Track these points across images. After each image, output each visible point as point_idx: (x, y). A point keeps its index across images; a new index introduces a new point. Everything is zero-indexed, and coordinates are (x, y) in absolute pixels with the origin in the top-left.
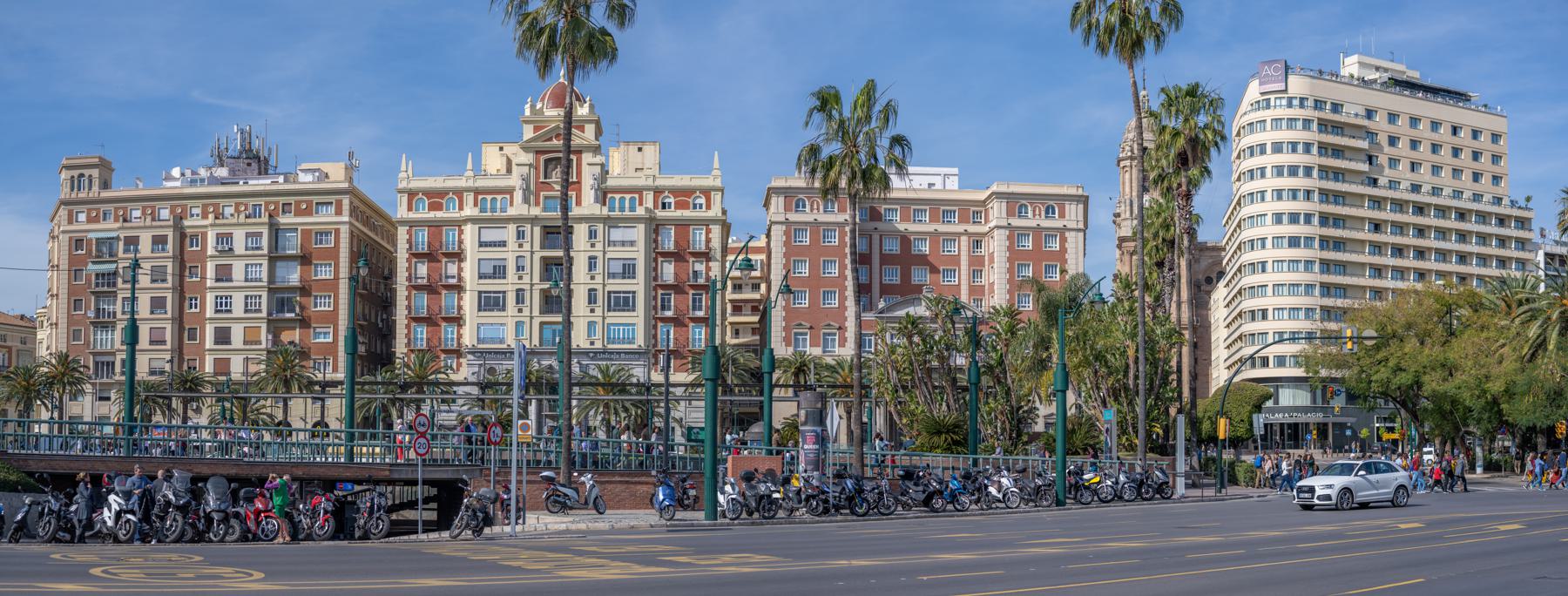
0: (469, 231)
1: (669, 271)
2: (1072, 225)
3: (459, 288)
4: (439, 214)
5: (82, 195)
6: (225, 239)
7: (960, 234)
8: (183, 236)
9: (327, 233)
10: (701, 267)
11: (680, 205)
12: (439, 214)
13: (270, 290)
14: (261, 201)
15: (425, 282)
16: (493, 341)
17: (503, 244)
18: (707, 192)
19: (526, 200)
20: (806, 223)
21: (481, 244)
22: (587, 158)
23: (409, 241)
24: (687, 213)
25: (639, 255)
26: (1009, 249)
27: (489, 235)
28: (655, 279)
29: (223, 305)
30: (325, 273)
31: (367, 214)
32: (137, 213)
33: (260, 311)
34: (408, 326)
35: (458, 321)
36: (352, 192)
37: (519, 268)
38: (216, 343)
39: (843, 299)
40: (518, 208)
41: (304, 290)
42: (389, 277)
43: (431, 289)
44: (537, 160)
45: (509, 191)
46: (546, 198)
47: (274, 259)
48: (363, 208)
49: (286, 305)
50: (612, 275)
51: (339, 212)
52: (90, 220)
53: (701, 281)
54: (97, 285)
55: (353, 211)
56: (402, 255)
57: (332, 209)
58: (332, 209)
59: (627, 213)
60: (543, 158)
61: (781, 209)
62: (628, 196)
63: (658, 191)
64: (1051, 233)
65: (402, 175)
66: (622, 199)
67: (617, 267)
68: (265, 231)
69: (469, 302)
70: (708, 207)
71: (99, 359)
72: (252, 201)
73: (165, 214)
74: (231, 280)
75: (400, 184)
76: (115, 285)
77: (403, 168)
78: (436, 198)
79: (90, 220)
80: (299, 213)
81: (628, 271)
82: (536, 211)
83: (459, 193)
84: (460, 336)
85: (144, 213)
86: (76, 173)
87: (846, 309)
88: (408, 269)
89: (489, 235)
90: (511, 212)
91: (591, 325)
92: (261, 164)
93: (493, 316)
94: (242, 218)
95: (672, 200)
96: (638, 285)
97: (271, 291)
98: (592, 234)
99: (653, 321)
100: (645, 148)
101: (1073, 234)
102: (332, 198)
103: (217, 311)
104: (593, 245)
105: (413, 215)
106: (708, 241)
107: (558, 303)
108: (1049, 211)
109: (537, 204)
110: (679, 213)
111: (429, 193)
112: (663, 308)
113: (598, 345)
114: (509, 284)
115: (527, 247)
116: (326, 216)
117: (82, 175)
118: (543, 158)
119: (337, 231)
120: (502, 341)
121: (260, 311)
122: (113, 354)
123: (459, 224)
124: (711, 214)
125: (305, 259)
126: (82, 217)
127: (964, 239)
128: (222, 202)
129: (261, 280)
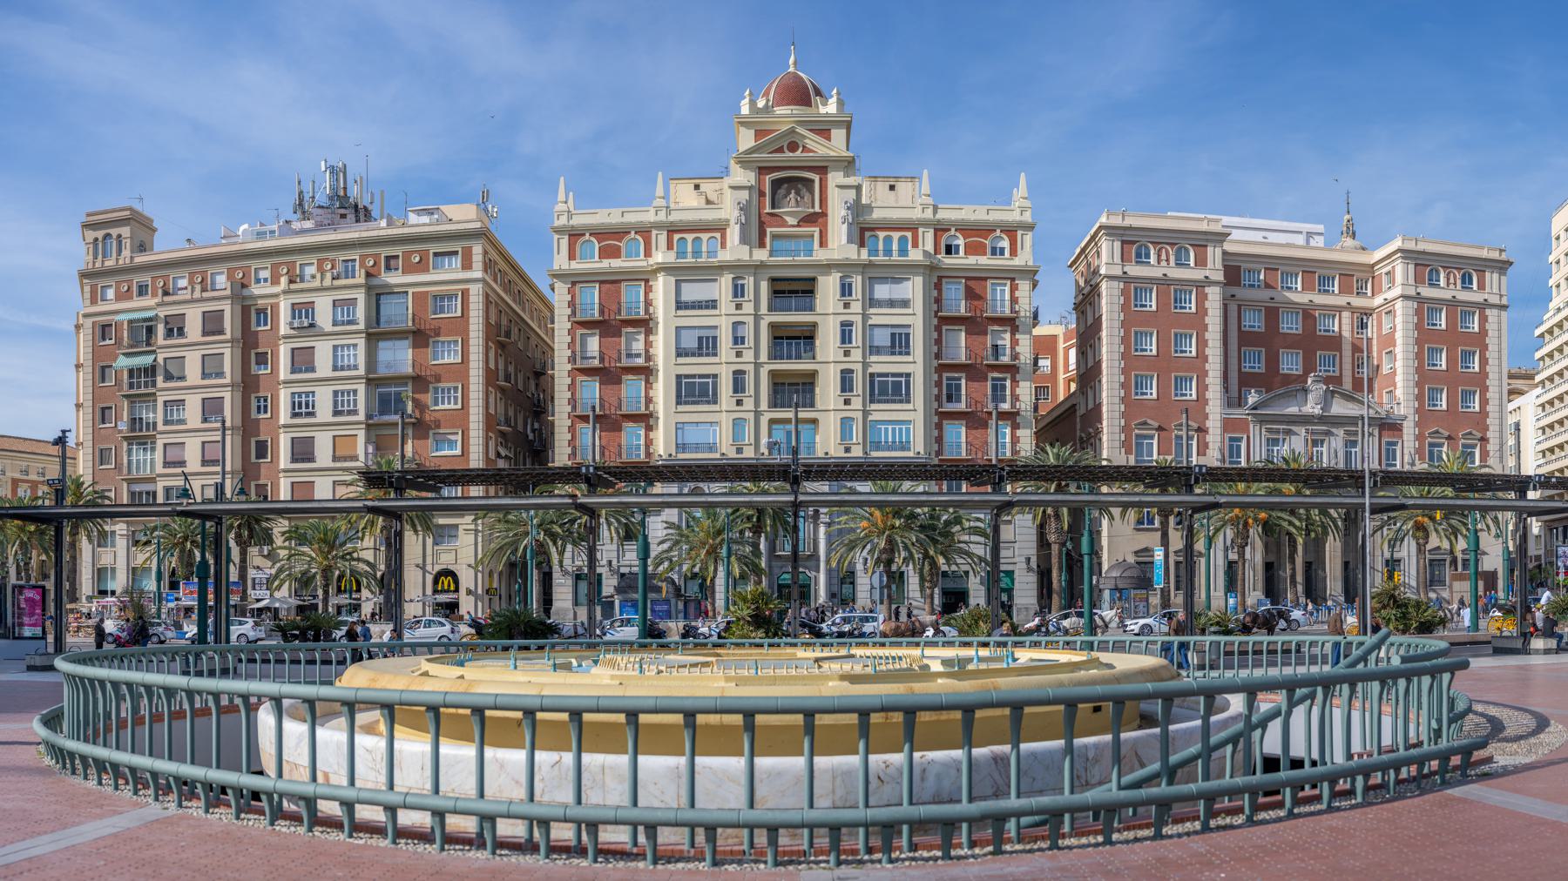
0: (662, 288)
1: (960, 345)
2: (1494, 300)
3: (647, 372)
4: (616, 263)
5: (110, 263)
6: (303, 311)
7: (1340, 309)
8: (246, 311)
9: (451, 297)
10: (1006, 340)
11: (972, 249)
12: (616, 263)
13: (369, 381)
14: (355, 255)
15: (596, 363)
16: (697, 448)
17: (712, 304)
18: (1011, 231)
19: (744, 240)
20: (1151, 280)
21: (680, 305)
22: (835, 178)
23: (572, 304)
24: (984, 261)
25: (915, 321)
26: (1418, 327)
27: (691, 292)
28: (938, 356)
29: (303, 408)
30: (449, 357)
31: (507, 276)
32: (183, 283)
33: (355, 412)
34: (572, 429)
35: (646, 419)
36: (481, 234)
37: (738, 340)
38: (294, 460)
39: (1202, 388)
40: (734, 250)
41: (420, 381)
42: (540, 374)
43: (607, 326)
44: (760, 181)
45: (720, 228)
46: (775, 237)
47: (374, 337)
48: (502, 265)
49: (394, 404)
50: (875, 350)
51: (467, 265)
52: (119, 297)
53: (1005, 359)
54: (131, 386)
55: (488, 265)
56: (562, 325)
57: (457, 262)
58: (457, 262)
59: (895, 257)
60: (768, 178)
61: (1117, 259)
62: (896, 235)
63: (940, 229)
64: (1469, 308)
65: (561, 207)
66: (888, 240)
67: (882, 338)
68: (361, 296)
69: (662, 392)
70: (1014, 253)
71: (137, 488)
72: (342, 256)
73: (222, 280)
74: (313, 370)
75: (550, 229)
76: (154, 384)
77: (561, 197)
78: (611, 239)
79: (119, 297)
80: (407, 270)
81: (899, 343)
82: (761, 255)
83: (645, 231)
84: (649, 443)
85: (191, 282)
86: (100, 234)
87: (1206, 402)
88: (571, 345)
89: (691, 292)
90: (725, 256)
91: (846, 423)
92: (362, 214)
93: (696, 412)
94: (328, 282)
95: (961, 242)
96: (914, 364)
97: (370, 382)
98: (846, 290)
99: (940, 418)
100: (900, 186)
101: (1495, 312)
102: (457, 246)
103: (295, 415)
104: (847, 305)
105: (575, 266)
106: (1014, 300)
107: (794, 390)
108: (1466, 281)
109: (762, 245)
110: (972, 260)
111: (601, 233)
112: (950, 399)
113: (857, 452)
114: (722, 365)
115: (748, 308)
116: (449, 272)
117: (108, 236)
118: (768, 178)
119: (465, 293)
120: (711, 448)
121: (355, 412)
122: (152, 480)
123: (645, 278)
124: (1018, 262)
125: (420, 337)
126: (111, 294)
127: (1346, 314)
128: (299, 260)
129: (356, 367)
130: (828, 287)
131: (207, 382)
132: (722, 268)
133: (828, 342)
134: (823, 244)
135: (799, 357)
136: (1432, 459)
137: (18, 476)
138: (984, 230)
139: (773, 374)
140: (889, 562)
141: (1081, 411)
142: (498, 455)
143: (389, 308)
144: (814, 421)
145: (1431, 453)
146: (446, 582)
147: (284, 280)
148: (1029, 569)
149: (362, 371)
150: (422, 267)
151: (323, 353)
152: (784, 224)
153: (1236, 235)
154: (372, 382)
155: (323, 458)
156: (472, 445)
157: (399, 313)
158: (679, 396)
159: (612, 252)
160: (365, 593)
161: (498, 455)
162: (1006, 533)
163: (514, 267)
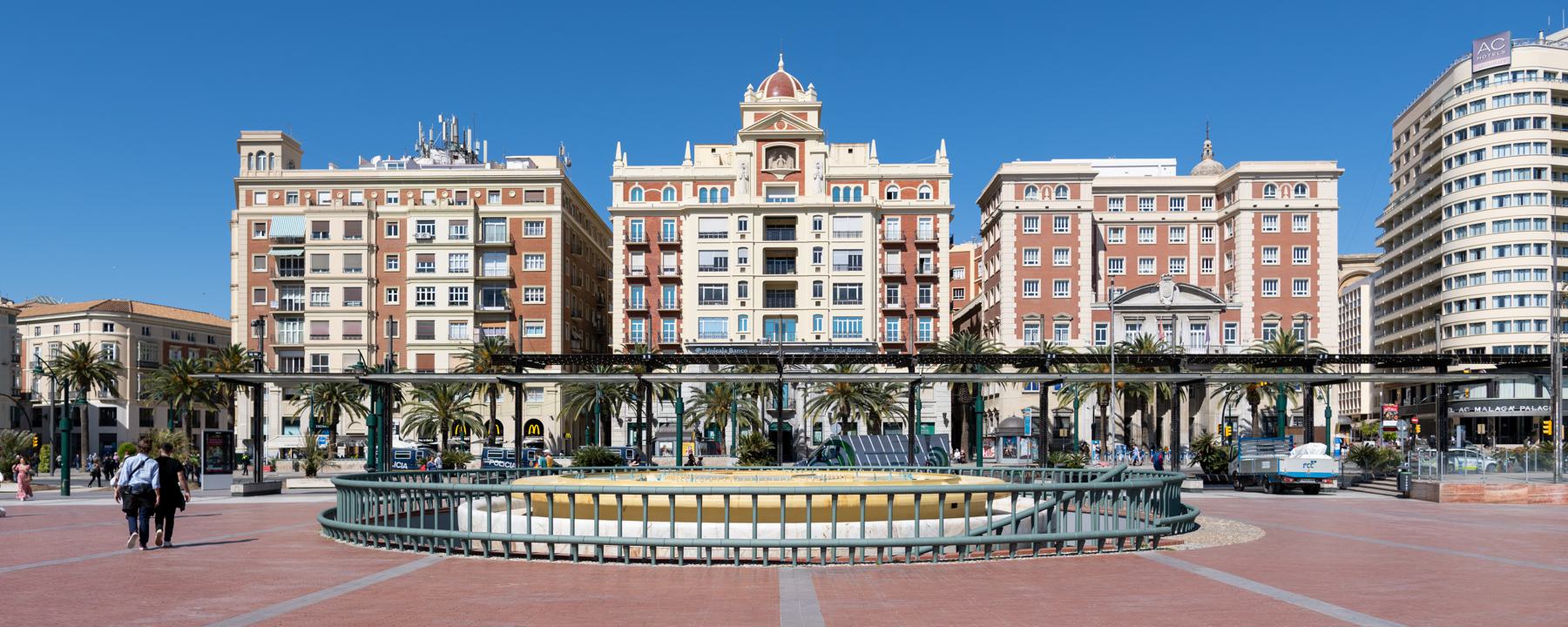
29: (426, 297)
37: (742, 260)
38: (419, 337)
47: (481, 251)
51: (550, 202)
52: (272, 202)
55: (565, 202)
70: (936, 196)
82: (760, 201)
87: (1078, 299)
95: (899, 190)
96: (867, 277)
107: (779, 295)
112: (889, 301)
114: (731, 277)
117: (261, 153)
119: (549, 221)
130: (804, 223)
131: (348, 275)
132: (732, 210)
133: (804, 261)
134: (802, 193)
135: (784, 272)
136: (1266, 337)
137: (169, 339)
138: (915, 181)
139: (766, 251)
140: (845, 419)
141: (985, 307)
142: (572, 338)
143: (492, 229)
144: (795, 317)
145: (1266, 333)
146: (534, 428)
147: (411, 202)
148: (946, 422)
149: (471, 274)
150: (516, 200)
151: (441, 258)
152: (775, 179)
153: (1102, 173)
154: (479, 283)
155: (451, 343)
156: (548, 332)
157: (497, 235)
158: (700, 298)
159: (656, 197)
160: (474, 437)
161: (572, 338)
162: (924, 395)
163: (584, 203)
